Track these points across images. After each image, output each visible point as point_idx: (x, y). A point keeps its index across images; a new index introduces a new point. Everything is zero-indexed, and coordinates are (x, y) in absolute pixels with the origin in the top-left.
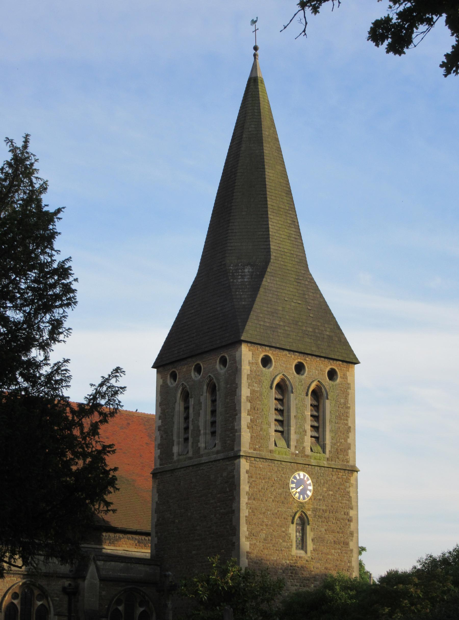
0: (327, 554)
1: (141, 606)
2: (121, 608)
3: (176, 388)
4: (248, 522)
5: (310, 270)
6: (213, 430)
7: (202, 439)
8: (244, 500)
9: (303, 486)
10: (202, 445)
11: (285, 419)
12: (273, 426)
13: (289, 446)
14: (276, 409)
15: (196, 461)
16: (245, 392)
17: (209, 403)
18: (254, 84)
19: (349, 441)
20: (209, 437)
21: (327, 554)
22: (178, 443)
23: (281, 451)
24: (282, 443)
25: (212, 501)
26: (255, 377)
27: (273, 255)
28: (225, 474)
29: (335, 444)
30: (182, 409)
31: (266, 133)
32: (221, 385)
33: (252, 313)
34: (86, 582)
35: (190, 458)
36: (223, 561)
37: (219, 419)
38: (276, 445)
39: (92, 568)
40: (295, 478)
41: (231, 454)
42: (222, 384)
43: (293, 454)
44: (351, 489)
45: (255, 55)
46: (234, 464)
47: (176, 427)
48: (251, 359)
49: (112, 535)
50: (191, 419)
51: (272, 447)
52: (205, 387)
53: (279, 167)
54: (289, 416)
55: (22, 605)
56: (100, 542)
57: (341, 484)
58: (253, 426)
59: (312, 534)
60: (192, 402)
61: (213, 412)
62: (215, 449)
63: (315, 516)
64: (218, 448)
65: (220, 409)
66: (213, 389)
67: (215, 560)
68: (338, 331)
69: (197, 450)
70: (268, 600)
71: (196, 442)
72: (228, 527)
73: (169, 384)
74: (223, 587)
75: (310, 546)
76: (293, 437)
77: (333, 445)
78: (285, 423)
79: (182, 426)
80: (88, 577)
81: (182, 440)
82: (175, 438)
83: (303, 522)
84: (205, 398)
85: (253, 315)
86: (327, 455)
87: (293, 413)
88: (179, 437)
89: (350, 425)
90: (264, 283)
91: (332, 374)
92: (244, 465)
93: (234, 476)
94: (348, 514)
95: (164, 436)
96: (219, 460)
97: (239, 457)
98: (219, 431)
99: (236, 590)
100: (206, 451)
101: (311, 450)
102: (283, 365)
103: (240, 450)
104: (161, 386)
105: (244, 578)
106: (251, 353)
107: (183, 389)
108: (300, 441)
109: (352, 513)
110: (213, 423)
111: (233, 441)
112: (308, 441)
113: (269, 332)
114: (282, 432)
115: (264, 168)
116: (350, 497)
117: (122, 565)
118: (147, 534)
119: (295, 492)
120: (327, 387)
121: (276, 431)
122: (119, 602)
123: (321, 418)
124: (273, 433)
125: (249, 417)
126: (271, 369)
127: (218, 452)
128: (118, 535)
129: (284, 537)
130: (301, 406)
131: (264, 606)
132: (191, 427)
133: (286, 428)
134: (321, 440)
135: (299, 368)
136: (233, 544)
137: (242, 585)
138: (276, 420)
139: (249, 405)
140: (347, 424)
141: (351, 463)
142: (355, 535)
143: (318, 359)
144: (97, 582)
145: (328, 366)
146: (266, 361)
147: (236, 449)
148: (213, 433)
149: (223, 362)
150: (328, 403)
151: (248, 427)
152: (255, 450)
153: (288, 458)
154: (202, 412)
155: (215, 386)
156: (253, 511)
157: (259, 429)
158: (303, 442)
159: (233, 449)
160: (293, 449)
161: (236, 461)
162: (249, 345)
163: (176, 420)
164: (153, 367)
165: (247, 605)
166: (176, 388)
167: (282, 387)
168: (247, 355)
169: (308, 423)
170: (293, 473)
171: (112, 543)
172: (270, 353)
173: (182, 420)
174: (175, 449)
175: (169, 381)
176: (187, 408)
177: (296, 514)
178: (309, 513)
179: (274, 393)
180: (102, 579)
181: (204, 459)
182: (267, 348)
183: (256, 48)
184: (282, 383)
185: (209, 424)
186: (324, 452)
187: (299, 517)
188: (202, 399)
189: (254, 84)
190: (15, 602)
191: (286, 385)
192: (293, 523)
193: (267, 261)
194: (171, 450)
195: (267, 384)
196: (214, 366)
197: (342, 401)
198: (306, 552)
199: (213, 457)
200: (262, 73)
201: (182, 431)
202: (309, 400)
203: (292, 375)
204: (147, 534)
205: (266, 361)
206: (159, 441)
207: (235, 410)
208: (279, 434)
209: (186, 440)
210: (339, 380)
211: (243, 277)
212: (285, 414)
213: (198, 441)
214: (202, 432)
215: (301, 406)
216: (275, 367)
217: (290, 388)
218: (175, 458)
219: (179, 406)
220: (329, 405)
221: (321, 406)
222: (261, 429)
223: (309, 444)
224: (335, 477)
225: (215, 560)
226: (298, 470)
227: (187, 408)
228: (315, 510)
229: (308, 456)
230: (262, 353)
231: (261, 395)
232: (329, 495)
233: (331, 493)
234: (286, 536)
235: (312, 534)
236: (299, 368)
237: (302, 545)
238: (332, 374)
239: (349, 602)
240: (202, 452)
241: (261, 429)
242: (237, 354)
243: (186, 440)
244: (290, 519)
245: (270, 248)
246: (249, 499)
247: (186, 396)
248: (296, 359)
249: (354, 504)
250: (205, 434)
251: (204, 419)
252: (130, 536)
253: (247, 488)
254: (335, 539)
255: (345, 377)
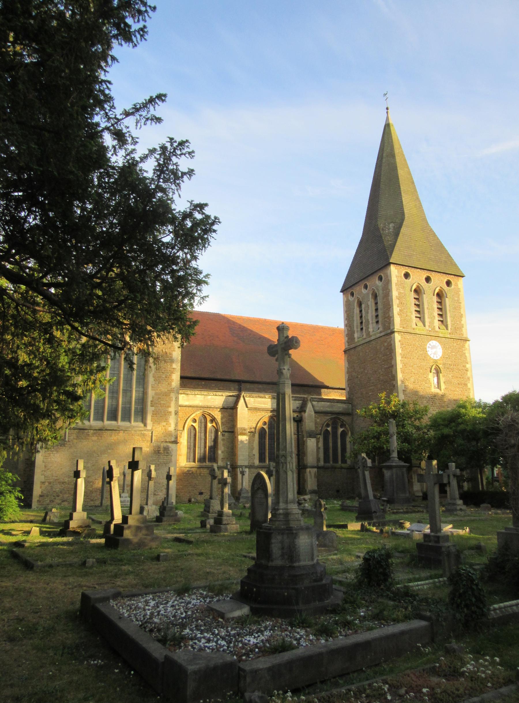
0: (454, 391)
1: (341, 427)
2: (329, 429)
3: (354, 301)
4: (403, 372)
5: (430, 224)
6: (376, 314)
7: (371, 326)
8: (399, 358)
9: (435, 351)
10: (371, 330)
11: (421, 304)
12: (414, 314)
13: (424, 325)
14: (415, 304)
15: (368, 340)
16: (395, 293)
17: (373, 304)
18: (387, 126)
19: (462, 322)
20: (375, 324)
21: (454, 391)
22: (357, 331)
23: (420, 328)
24: (420, 324)
25: (379, 362)
26: (400, 284)
27: (406, 216)
28: (386, 344)
29: (454, 325)
30: (358, 312)
31: (396, 151)
32: (380, 294)
33: (396, 247)
34: (306, 413)
35: (365, 339)
36: (388, 396)
37: (380, 313)
38: (416, 325)
39: (309, 405)
40: (430, 344)
41: (389, 331)
42: (381, 292)
43: (427, 330)
44: (466, 352)
45: (387, 112)
46: (391, 337)
47: (355, 322)
48: (397, 274)
49: (326, 390)
50: (363, 316)
51: (414, 326)
52: (371, 296)
53: (406, 169)
54: (423, 308)
55: (269, 429)
56: (320, 394)
57: (459, 348)
58: (402, 312)
59: (444, 379)
60: (363, 306)
61: (377, 310)
62: (379, 331)
63: (445, 368)
64: (381, 329)
65: (380, 306)
66: (375, 296)
67: (383, 395)
68: (450, 258)
69: (368, 334)
70: (419, 419)
71: (368, 328)
72: (390, 376)
73: (350, 299)
74: (388, 411)
75: (443, 386)
76: (427, 320)
77: (452, 325)
78: (421, 312)
79: (359, 321)
80: (307, 411)
81: (359, 329)
82: (355, 329)
83: (438, 372)
84: (371, 302)
85: (396, 248)
86: (449, 331)
87: (426, 306)
88: (357, 328)
89: (462, 313)
90: (402, 231)
91: (448, 283)
92: (397, 337)
93: (391, 345)
94: (465, 366)
95: (349, 329)
96: (381, 336)
97: (394, 332)
98: (380, 319)
99: (398, 414)
100: (374, 333)
101: (439, 328)
102: (418, 278)
103: (394, 328)
104: (346, 302)
105: (402, 405)
106: (397, 270)
107: (358, 300)
108: (432, 323)
109: (468, 366)
110: (377, 316)
111: (389, 323)
112: (437, 323)
113: (407, 258)
114: (420, 318)
115: (397, 170)
116: (466, 356)
117: (328, 403)
118: (344, 389)
119: (430, 352)
120: (446, 291)
121: (416, 317)
122: (328, 425)
123: (443, 310)
124: (415, 318)
125: (398, 309)
126: (410, 280)
127: (381, 332)
128: (329, 390)
129: (426, 381)
130: (430, 302)
131: (417, 423)
132: (364, 321)
133: (422, 315)
134: (444, 322)
135: (428, 279)
136: (394, 386)
137: (401, 410)
138: (416, 311)
139: (398, 301)
140: (460, 313)
141: (464, 336)
142: (471, 379)
143: (439, 274)
144: (313, 413)
145: (446, 278)
146: (407, 276)
147: (391, 328)
148: (377, 322)
149: (380, 279)
150: (447, 300)
151: (398, 315)
152: (404, 328)
153: (424, 333)
154: (370, 311)
155: (376, 294)
156: (405, 365)
157: (405, 315)
158: (433, 323)
159: (390, 329)
160: (427, 327)
161: (392, 336)
162: (395, 265)
163: (355, 319)
164: (341, 292)
165: (406, 422)
166: (354, 301)
167: (417, 291)
168: (395, 273)
169: (436, 312)
170: (429, 341)
171: (327, 395)
172: (409, 270)
173: (359, 318)
174: (356, 335)
175: (350, 298)
176: (361, 311)
177: (432, 366)
178: (440, 366)
179: (413, 295)
180: (316, 412)
181: (372, 338)
182: (407, 268)
183: (387, 109)
184: (417, 289)
185: (374, 317)
186: (447, 329)
187: (435, 369)
188: (369, 303)
189: (387, 126)
190: (265, 427)
191: (420, 290)
192: (431, 372)
193: (403, 220)
194: (354, 336)
195: (408, 289)
196: (375, 283)
197: (456, 299)
198: (441, 390)
199: (378, 335)
200: (391, 122)
201: (359, 324)
202: (435, 299)
203: (423, 283)
204: (344, 389)
205: (407, 276)
206: (346, 333)
207: (389, 305)
208: (418, 319)
209: (362, 329)
210: (453, 287)
211: (389, 229)
212: (421, 306)
213: (369, 328)
214: (370, 322)
215: (430, 302)
216: (413, 279)
217: (423, 291)
218: (356, 340)
219: (357, 310)
220: (448, 302)
221: (443, 302)
222: (407, 316)
223: (438, 325)
224: (455, 344)
225: (383, 395)
226: (431, 340)
227: (361, 311)
228: (444, 364)
229: (437, 332)
230: (404, 270)
231: (405, 295)
232: (452, 355)
233: (453, 354)
234: (427, 381)
235: (444, 379)
236: (428, 279)
237: (439, 387)
238: (448, 283)
239: (478, 416)
240: (371, 334)
241: (407, 316)
242: (388, 272)
243: (362, 329)
244: (429, 370)
245: (404, 212)
246: (402, 358)
247: (360, 304)
248: (425, 274)
249: (468, 360)
250: (372, 323)
251: (370, 315)
252: (336, 390)
253: (400, 351)
254: (458, 382)
255: (456, 285)
